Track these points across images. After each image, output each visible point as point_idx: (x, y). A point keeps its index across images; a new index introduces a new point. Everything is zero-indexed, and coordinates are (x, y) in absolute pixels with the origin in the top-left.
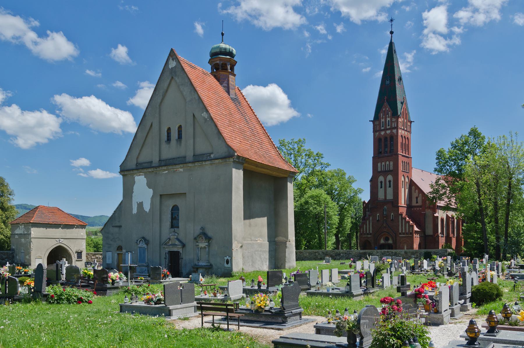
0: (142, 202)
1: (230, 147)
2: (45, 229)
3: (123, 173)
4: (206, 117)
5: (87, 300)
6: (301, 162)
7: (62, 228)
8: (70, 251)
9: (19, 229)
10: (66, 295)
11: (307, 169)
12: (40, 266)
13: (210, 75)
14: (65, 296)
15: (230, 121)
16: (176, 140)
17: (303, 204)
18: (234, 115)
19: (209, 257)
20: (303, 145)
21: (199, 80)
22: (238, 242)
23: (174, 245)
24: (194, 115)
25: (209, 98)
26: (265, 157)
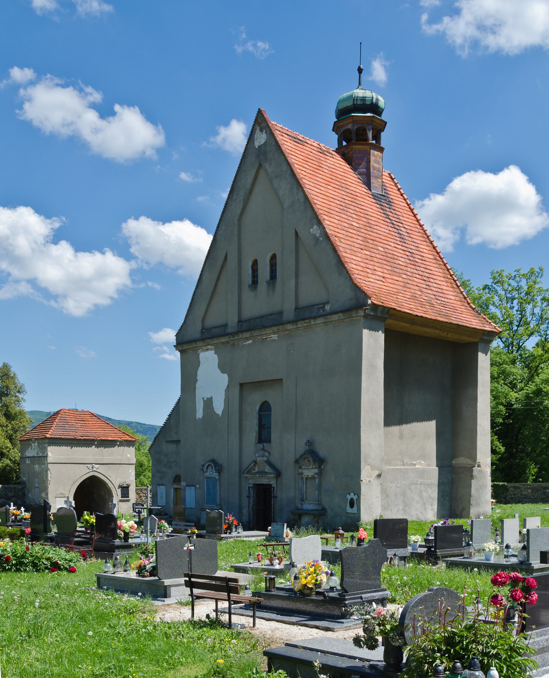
0: (212, 398)
1: (360, 289)
2: (69, 448)
3: (180, 349)
4: (318, 235)
5: (68, 567)
6: (533, 314)
7: (97, 446)
8: (110, 485)
9: (31, 449)
10: (32, 556)
11: (543, 326)
12: (10, 507)
13: (334, 153)
14: (30, 558)
15: (365, 240)
16: (267, 281)
17: (531, 395)
18: (375, 227)
19: (319, 494)
20: (538, 280)
21: (310, 164)
22: (373, 468)
23: (263, 473)
24: (296, 233)
25: (326, 197)
26: (432, 305)
